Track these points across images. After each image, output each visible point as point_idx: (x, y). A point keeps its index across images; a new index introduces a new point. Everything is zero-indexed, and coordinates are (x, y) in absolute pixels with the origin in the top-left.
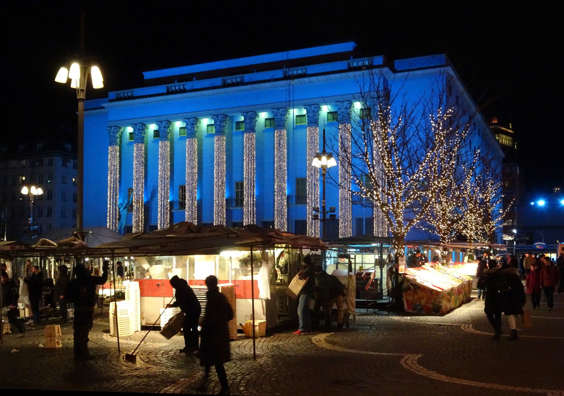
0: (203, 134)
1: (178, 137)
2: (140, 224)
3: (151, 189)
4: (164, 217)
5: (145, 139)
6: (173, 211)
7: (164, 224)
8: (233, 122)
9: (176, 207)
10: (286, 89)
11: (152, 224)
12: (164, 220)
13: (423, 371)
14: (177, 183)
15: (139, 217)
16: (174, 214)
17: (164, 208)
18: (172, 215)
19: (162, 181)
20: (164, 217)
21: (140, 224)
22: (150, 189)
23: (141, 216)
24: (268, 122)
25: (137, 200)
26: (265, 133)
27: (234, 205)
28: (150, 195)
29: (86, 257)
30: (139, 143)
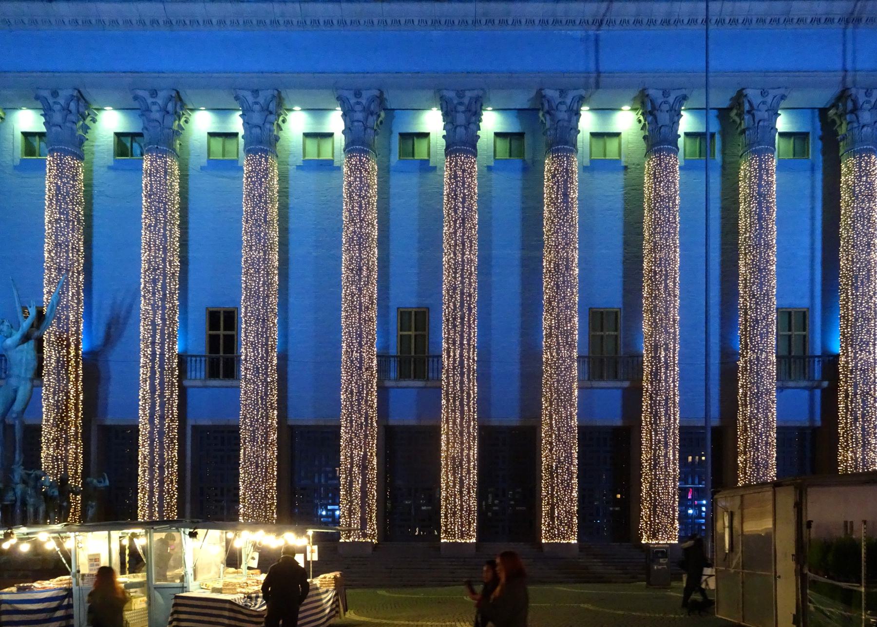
0: (291, 160)
1: (204, 161)
2: (72, 414)
3: (106, 313)
4: (162, 396)
5: (86, 147)
6: (186, 383)
7: (162, 418)
8: (391, 132)
9: (197, 376)
10: (586, 39)
11: (110, 421)
12: (162, 405)
13: (46, 537)
14: (202, 301)
15: (67, 393)
16: (190, 391)
17: (161, 366)
18: (183, 392)
19: (155, 281)
20: (162, 396)
21: (72, 414)
22: (102, 315)
23: (75, 388)
24: (503, 145)
25: (59, 338)
26: (494, 175)
27: (393, 375)
28: (100, 332)
29: (829, 384)
30: (67, 153)
